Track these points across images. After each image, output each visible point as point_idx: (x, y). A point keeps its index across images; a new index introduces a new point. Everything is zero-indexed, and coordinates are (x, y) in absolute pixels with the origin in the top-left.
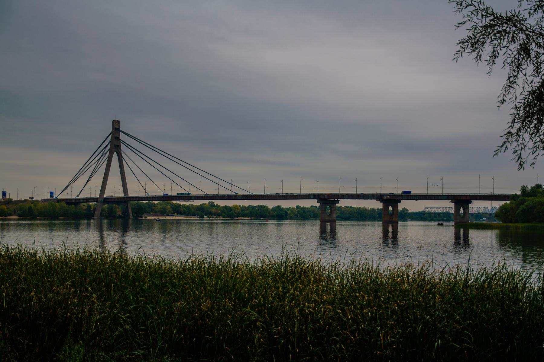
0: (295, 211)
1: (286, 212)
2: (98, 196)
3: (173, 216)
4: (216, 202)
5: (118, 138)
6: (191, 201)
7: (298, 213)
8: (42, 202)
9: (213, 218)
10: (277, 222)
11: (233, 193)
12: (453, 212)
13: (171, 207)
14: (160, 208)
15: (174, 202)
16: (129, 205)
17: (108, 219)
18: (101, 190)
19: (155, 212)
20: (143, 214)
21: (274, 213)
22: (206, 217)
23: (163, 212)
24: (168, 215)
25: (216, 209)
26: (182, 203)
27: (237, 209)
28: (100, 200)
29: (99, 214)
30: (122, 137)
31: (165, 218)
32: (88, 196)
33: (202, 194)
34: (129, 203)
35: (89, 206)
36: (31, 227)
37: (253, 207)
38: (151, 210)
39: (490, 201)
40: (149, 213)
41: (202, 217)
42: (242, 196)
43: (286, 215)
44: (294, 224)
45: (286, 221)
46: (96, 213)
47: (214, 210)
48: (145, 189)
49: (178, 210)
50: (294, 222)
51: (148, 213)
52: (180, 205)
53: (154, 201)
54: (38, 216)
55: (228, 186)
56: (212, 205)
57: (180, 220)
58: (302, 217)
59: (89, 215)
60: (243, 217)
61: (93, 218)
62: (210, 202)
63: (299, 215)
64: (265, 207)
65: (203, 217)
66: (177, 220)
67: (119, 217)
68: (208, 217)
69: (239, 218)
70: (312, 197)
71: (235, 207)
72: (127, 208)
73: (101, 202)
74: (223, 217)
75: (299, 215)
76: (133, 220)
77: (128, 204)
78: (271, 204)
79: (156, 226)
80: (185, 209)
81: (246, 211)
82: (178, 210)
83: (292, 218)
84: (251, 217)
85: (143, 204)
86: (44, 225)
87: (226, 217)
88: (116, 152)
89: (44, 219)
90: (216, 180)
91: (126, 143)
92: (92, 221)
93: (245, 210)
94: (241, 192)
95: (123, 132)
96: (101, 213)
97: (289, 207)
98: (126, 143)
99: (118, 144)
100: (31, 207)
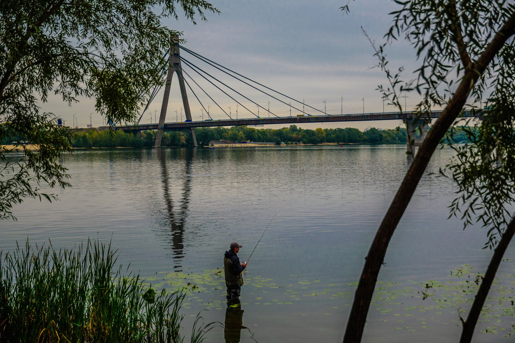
0: (392, 134)
1: (381, 136)
2: (158, 122)
3: (245, 143)
4: (299, 126)
5: (177, 55)
6: (260, 125)
7: (396, 136)
8: (100, 129)
9: (292, 144)
10: (371, 147)
13: (244, 133)
14: (231, 134)
15: (249, 127)
16: (193, 132)
17: (171, 148)
18: (161, 115)
19: (226, 139)
20: (209, 142)
21: (366, 137)
22: (283, 144)
23: (234, 139)
24: (240, 142)
25: (297, 134)
26: (258, 128)
27: (321, 133)
28: (160, 127)
29: (160, 143)
30: (182, 53)
31: (234, 145)
32: (148, 122)
33: (272, 116)
34: (193, 129)
35: (149, 135)
36: (91, 158)
37: (340, 130)
38: (221, 136)
40: (217, 140)
41: (278, 143)
42: (316, 118)
43: (381, 139)
44: (368, 149)
45: (380, 145)
46: (157, 141)
47: (294, 135)
48: (208, 113)
49: (251, 136)
50: (395, 146)
51: (216, 140)
53: (224, 127)
54: (94, 146)
55: (300, 107)
56: (294, 129)
57: (255, 147)
58: (401, 141)
59: (149, 144)
60: (330, 142)
61: (153, 147)
62: (291, 126)
63: (397, 138)
64: (355, 129)
65: (280, 144)
66: (251, 147)
67: (183, 146)
68: (286, 143)
69: (323, 144)
70: (397, 117)
71: (319, 130)
72: (191, 135)
73: (161, 129)
74: (304, 143)
75: (397, 138)
76: (198, 148)
77: (192, 131)
78: (362, 127)
79: (229, 155)
80: (259, 134)
81: (332, 136)
82: (251, 136)
83: (388, 142)
84: (338, 142)
85: (211, 131)
86: (103, 156)
87: (308, 143)
88: (176, 71)
89: (101, 149)
90: (288, 101)
92: (153, 151)
93: (331, 135)
94: (315, 114)
95: (181, 48)
96: (162, 141)
97: (369, 129)
99: (178, 62)
100: (85, 136)
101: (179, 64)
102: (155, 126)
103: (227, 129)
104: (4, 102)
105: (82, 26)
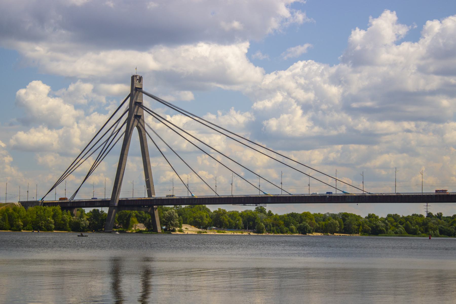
4: (268, 207)
11: (262, 193)
12: (109, 208)
30: (146, 102)
33: (284, 194)
39: (425, 204)
52: (224, 212)
53: (166, 206)
55: (330, 181)
91: (61, 177)
98: (61, 177)
101: (142, 117)
102: (104, 203)
103: (169, 207)
104: (82, 221)
105: (30, 210)
